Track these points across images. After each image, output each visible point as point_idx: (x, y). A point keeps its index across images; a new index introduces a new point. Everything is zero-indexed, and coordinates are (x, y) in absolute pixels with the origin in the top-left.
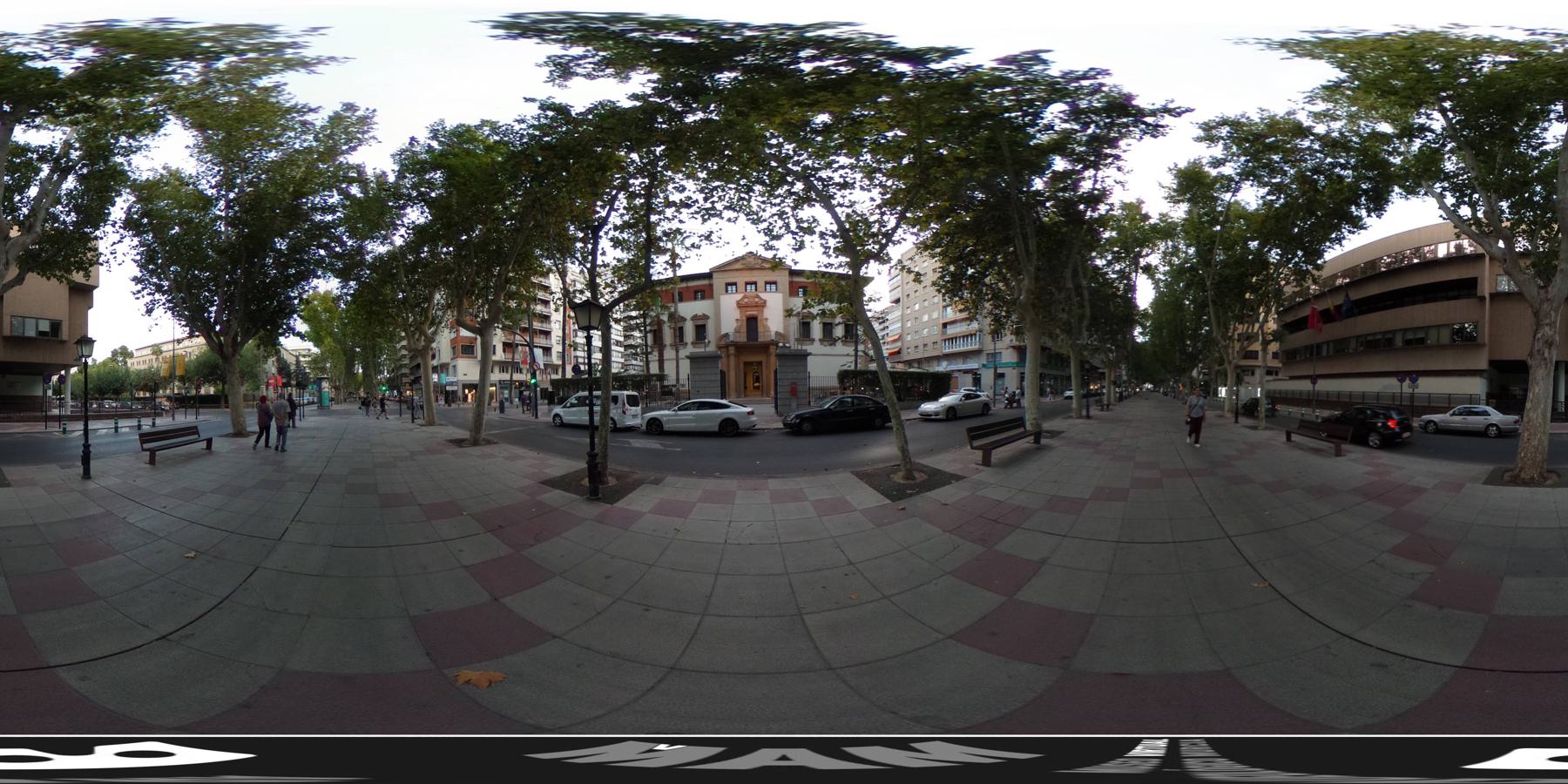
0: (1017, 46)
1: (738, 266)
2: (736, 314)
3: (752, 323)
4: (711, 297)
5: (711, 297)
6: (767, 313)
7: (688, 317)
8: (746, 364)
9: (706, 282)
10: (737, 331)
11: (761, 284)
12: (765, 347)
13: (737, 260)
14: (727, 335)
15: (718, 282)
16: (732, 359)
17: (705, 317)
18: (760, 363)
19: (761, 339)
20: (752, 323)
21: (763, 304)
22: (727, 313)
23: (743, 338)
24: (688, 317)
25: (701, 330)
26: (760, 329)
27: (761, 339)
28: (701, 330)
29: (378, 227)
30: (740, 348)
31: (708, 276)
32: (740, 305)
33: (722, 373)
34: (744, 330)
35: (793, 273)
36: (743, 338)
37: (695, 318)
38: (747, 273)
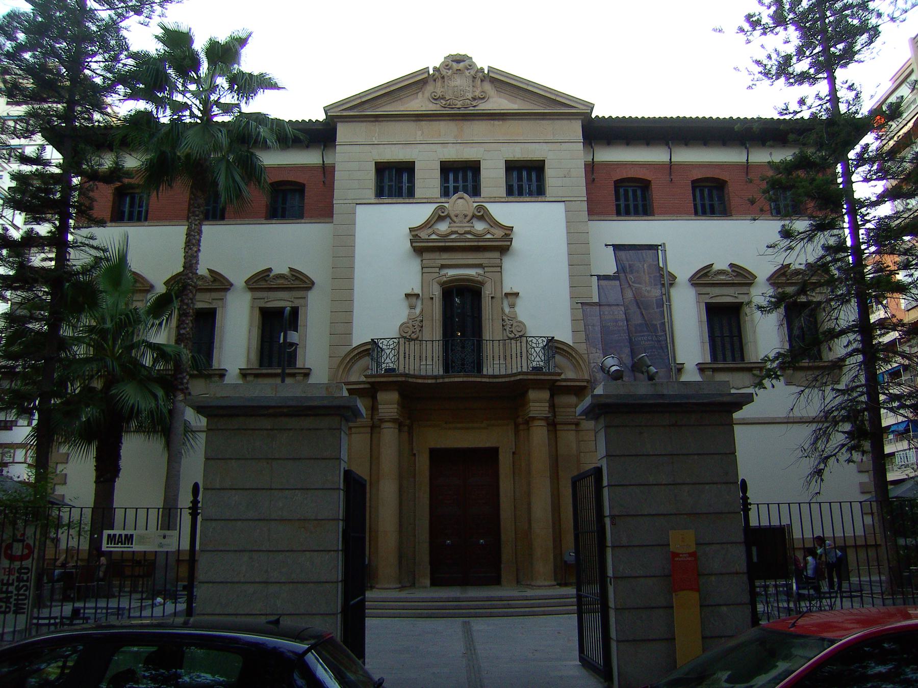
0: (207, 39)
1: (419, 103)
2: (409, 275)
3: (462, 309)
4: (326, 212)
5: (326, 212)
6: (515, 274)
7: (238, 278)
8: (436, 455)
9: (310, 158)
10: (409, 336)
11: (493, 176)
12: (507, 399)
13: (417, 83)
14: (372, 349)
15: (354, 159)
16: (389, 436)
17: (299, 282)
18: (492, 454)
19: (495, 366)
20: (462, 309)
21: (501, 244)
22: (374, 273)
23: (428, 363)
24: (238, 277)
25: (277, 327)
26: (491, 330)
27: (495, 366)
28: (277, 327)
29: (877, 235)
30: (417, 398)
31: (320, 135)
32: (422, 246)
33: (356, 490)
34: (434, 331)
35: (601, 132)
36: (428, 363)
37: (261, 282)
38: (446, 129)
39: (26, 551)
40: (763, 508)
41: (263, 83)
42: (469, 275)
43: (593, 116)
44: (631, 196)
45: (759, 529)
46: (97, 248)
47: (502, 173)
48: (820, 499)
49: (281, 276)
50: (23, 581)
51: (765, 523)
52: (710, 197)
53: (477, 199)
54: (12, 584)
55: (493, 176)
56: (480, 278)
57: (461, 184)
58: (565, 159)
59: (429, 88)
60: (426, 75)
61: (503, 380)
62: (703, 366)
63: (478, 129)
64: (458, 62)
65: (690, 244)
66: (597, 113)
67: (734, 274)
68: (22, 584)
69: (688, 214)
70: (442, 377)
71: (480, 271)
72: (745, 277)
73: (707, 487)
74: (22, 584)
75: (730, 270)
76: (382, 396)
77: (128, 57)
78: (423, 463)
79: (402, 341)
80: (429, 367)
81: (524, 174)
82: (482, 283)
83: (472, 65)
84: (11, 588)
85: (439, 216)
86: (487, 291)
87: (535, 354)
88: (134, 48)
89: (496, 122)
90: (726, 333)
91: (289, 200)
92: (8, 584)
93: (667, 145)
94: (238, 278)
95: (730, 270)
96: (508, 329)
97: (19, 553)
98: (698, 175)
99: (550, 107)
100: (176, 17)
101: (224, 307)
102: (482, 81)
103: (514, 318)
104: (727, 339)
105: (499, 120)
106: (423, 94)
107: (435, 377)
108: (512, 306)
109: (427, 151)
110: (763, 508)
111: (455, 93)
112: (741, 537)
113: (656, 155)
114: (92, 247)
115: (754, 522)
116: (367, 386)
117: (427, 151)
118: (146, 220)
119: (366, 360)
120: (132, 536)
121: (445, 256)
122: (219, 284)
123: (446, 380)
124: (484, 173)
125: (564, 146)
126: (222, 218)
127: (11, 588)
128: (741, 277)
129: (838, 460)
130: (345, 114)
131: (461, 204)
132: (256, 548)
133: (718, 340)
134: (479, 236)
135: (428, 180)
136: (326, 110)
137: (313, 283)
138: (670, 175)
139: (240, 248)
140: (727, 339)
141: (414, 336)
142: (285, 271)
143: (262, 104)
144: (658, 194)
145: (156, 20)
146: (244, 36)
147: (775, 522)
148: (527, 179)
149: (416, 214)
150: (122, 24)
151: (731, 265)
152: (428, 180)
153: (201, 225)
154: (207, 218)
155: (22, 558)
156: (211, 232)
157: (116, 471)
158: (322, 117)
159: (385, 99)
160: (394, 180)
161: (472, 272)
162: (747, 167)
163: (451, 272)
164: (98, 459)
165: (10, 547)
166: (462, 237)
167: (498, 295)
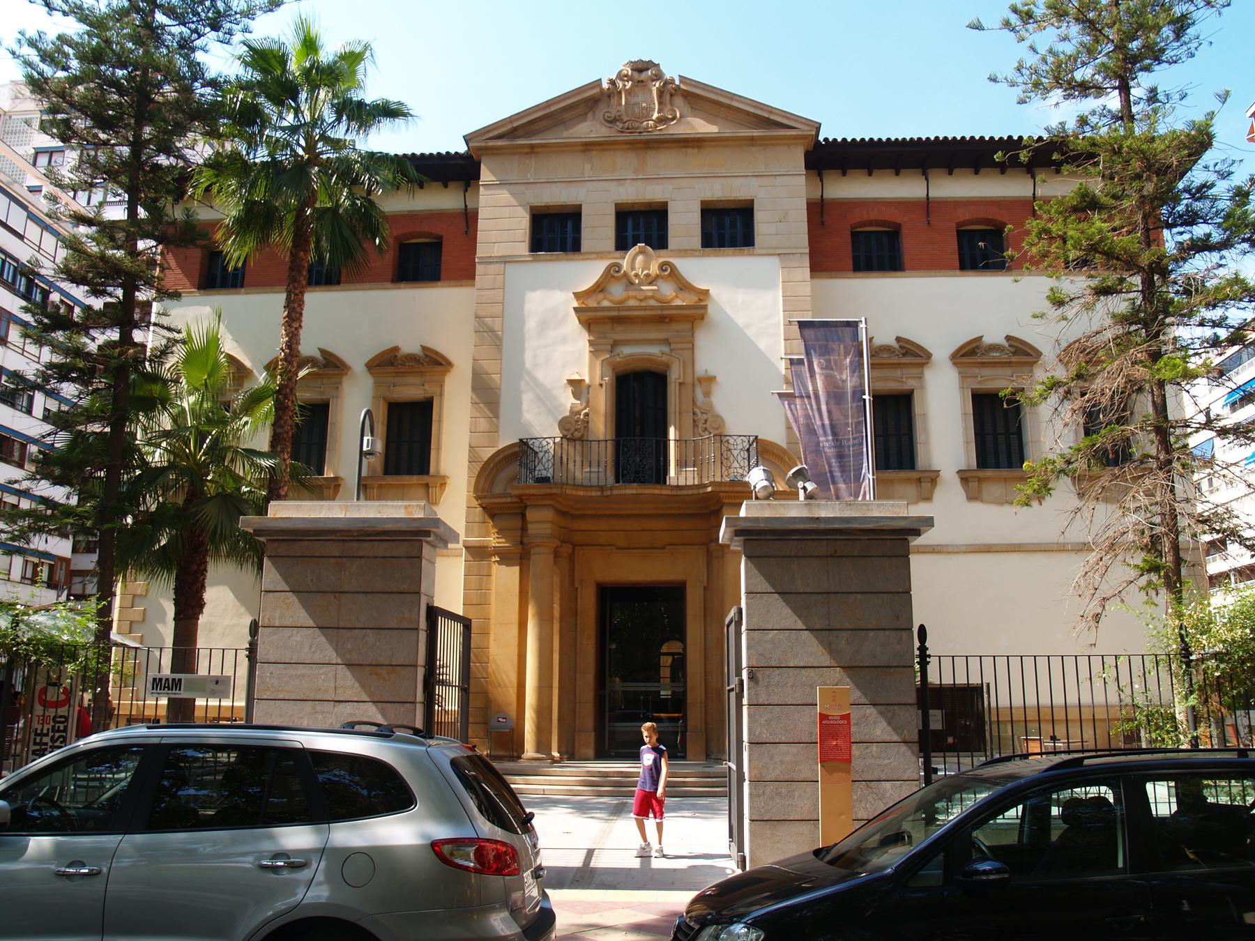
7: (356, 360)
11: (685, 223)
13: (589, 101)
20: (641, 402)
31: (455, 171)
34: (601, 427)
35: (829, 158)
36: (593, 470)
38: (625, 163)
39: (62, 697)
40: (947, 663)
41: (390, 111)
42: (650, 355)
43: (821, 138)
44: (870, 247)
45: (941, 690)
46: (169, 329)
47: (696, 218)
48: (1094, 651)
49: (995, 348)
50: (59, 731)
51: (948, 680)
52: (982, 246)
53: (662, 252)
54: (47, 735)
55: (685, 223)
56: (664, 358)
57: (642, 232)
58: (782, 197)
59: (602, 110)
60: (597, 90)
61: (690, 492)
62: (968, 474)
63: (665, 162)
64: (640, 71)
65: (933, 309)
66: (826, 134)
67: (1012, 350)
68: (57, 735)
69: (951, 268)
70: (611, 489)
71: (666, 349)
72: (1028, 354)
73: (871, 634)
74: (57, 735)
75: (1006, 344)
76: (531, 515)
77: (203, 86)
78: (588, 600)
79: (565, 442)
80: (594, 476)
81: (642, 220)
82: (668, 366)
83: (659, 76)
84: (45, 739)
85: (612, 274)
86: (674, 376)
87: (739, 459)
88: (211, 74)
89: (690, 151)
90: (1001, 430)
91: (429, 256)
92: (42, 735)
93: (925, 174)
94: (356, 360)
95: (1006, 344)
96: (701, 425)
97: (55, 699)
98: (963, 215)
99: (761, 126)
100: (272, 29)
101: (922, 387)
102: (671, 95)
103: (708, 410)
104: (1001, 439)
105: (693, 147)
106: (594, 114)
107: (602, 488)
108: (707, 394)
109: (598, 195)
110: (947, 663)
111: (617, 115)
112: (912, 697)
113: (908, 188)
114: (163, 327)
115: (933, 678)
116: (515, 500)
117: (598, 195)
118: (242, 286)
119: (514, 468)
120: (180, 680)
121: (619, 328)
122: (331, 366)
123: (615, 492)
124: (672, 219)
125: (780, 180)
126: (338, 283)
127: (45, 739)
128: (1021, 353)
129: (1122, 601)
130: (491, 143)
131: (638, 261)
132: (319, 697)
133: (989, 438)
134: (665, 304)
135: (598, 228)
136: (467, 139)
137: (929, 355)
138: (928, 215)
139: (355, 320)
140: (1001, 439)
141: (577, 435)
142: (891, 341)
143: (386, 139)
144: (909, 245)
145: (238, 37)
146: (358, 50)
147: (961, 680)
148: (729, 227)
149: (587, 272)
150: (197, 43)
151: (1008, 338)
152: (598, 228)
153: (302, 293)
154: (310, 283)
155: (57, 705)
156: (316, 301)
157: (200, 605)
158: (462, 148)
159: (544, 123)
160: (555, 232)
161: (654, 350)
162: (928, 206)
163: (627, 351)
164: (177, 590)
165: (44, 691)
166: (643, 304)
167: (689, 380)
